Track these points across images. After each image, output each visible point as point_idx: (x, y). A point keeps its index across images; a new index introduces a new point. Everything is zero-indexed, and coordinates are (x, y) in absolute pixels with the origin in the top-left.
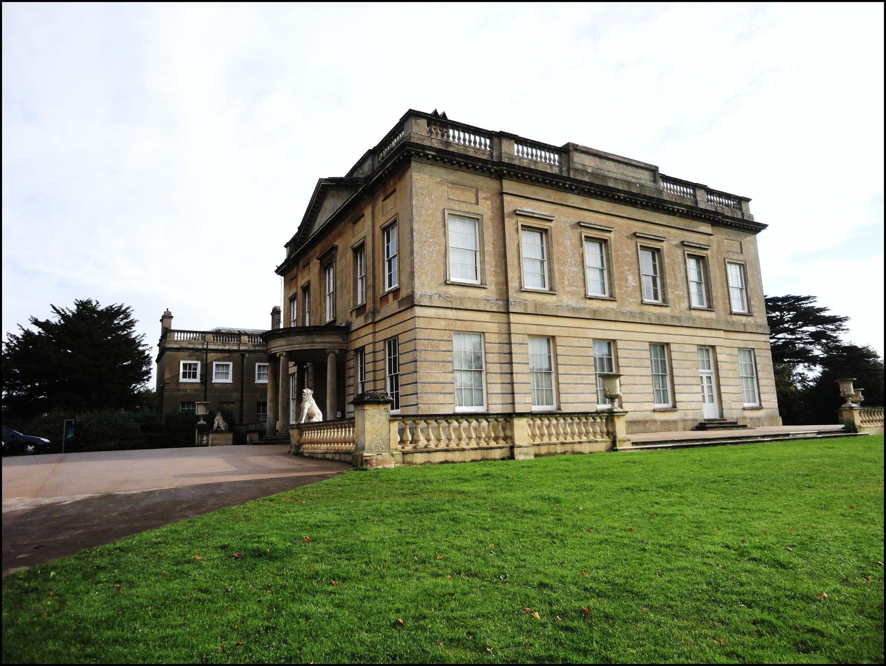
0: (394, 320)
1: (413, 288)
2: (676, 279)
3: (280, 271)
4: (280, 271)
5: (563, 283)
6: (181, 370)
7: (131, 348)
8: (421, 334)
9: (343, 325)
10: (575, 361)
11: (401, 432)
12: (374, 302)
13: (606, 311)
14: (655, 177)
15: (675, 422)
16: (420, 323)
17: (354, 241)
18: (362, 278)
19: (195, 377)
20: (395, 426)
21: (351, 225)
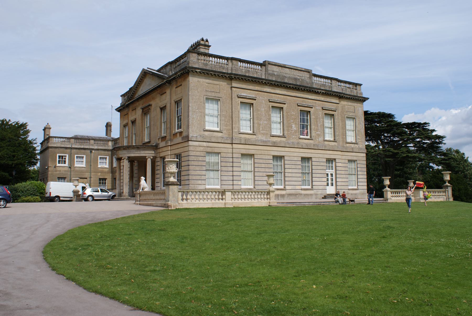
0: (180, 146)
1: (188, 132)
2: (317, 126)
3: (119, 110)
4: (119, 110)
5: (259, 129)
6: (58, 159)
7: (27, 147)
8: (191, 153)
9: (154, 145)
10: (263, 165)
11: (182, 196)
12: (170, 136)
13: (280, 142)
14: (310, 75)
15: (311, 195)
16: (191, 148)
17: (162, 104)
18: (164, 122)
19: (65, 163)
20: (180, 194)
21: (158, 95)
